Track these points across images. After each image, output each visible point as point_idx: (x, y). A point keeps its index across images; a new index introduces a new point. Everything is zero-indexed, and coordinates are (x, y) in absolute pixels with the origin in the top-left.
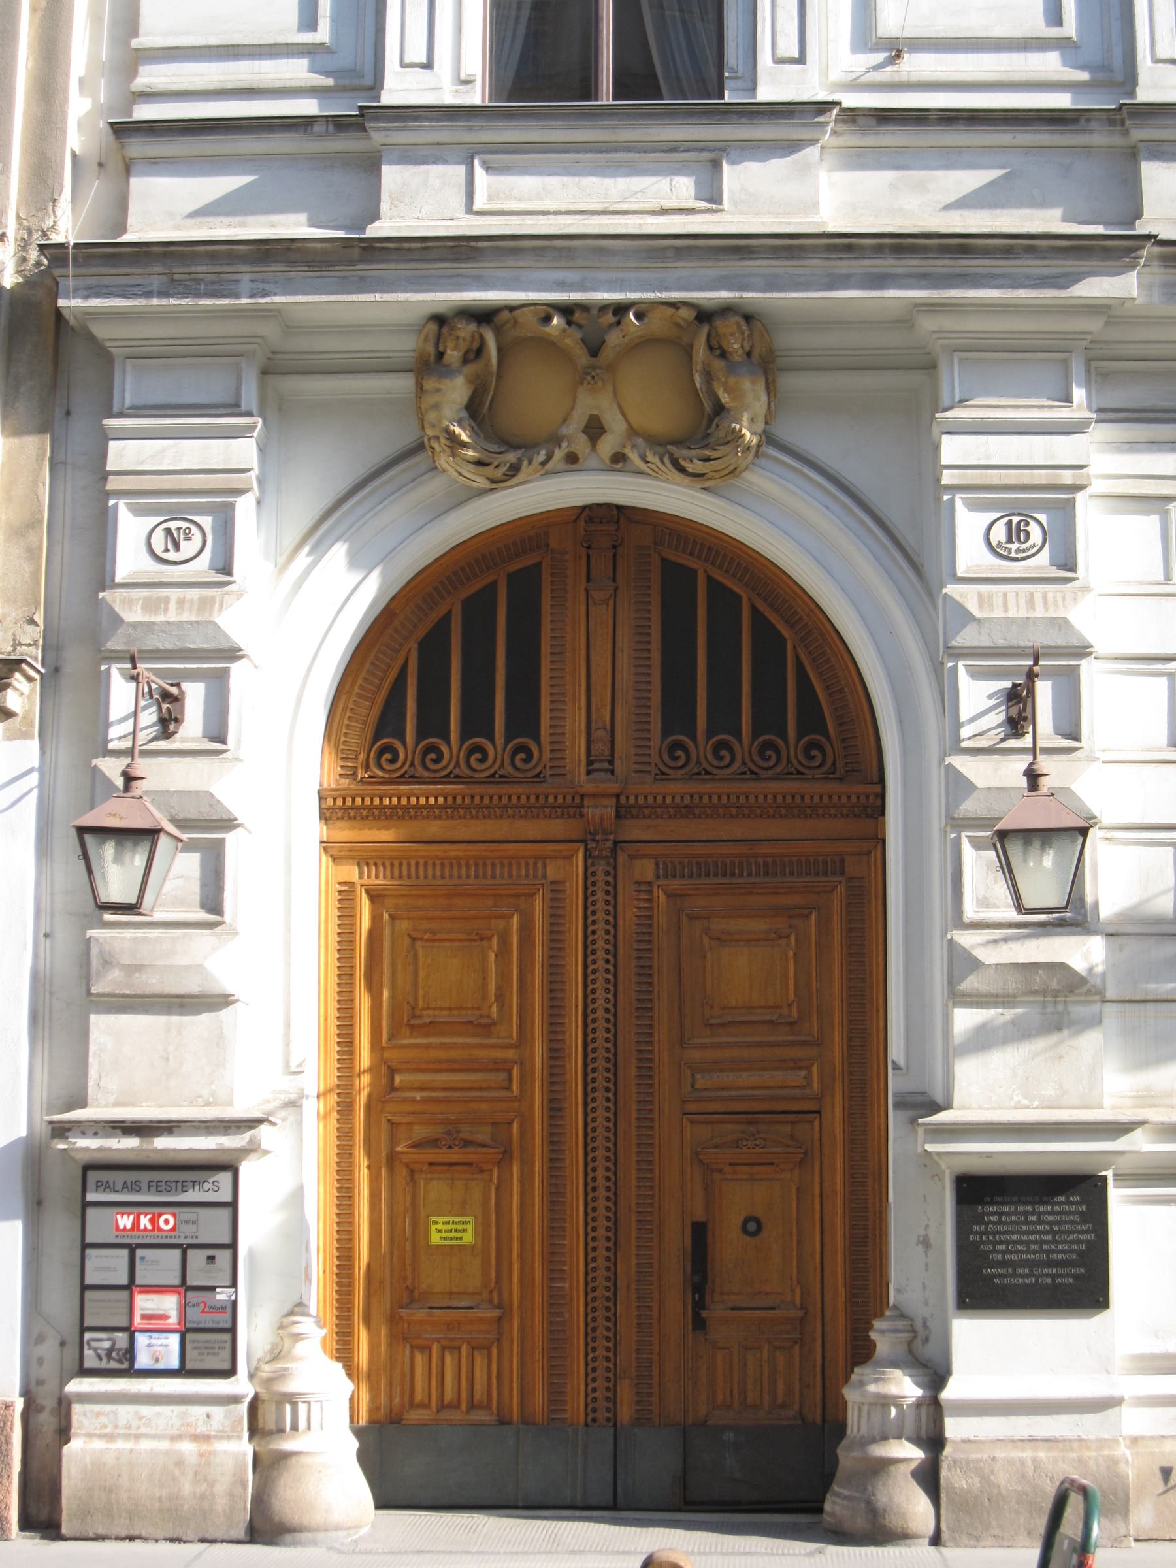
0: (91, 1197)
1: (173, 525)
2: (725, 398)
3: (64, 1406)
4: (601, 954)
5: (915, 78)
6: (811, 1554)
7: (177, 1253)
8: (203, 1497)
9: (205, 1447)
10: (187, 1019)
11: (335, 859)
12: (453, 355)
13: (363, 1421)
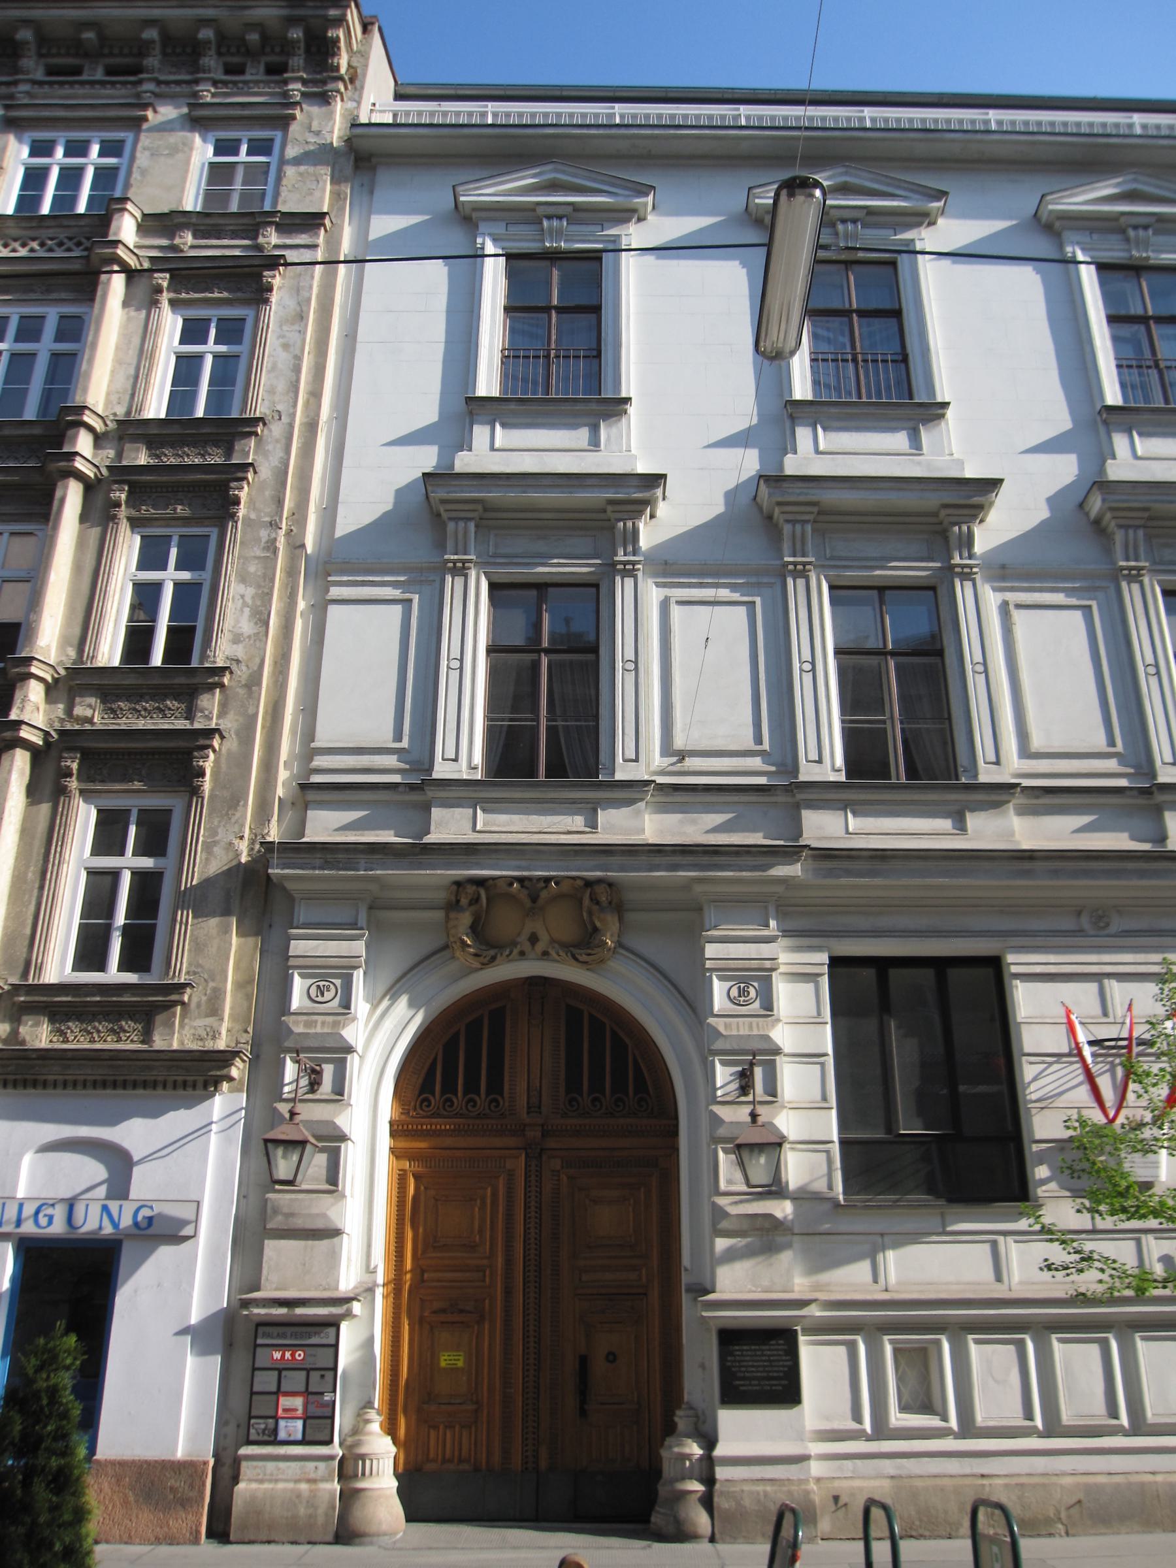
0: (259, 1341)
1: (321, 984)
2: (598, 924)
3: (237, 1462)
4: (533, 1208)
5: (691, 769)
6: (644, 1548)
7: (304, 1373)
8: (310, 1516)
9: (314, 1487)
10: (317, 1242)
11: (397, 1157)
12: (464, 901)
13: (400, 1470)
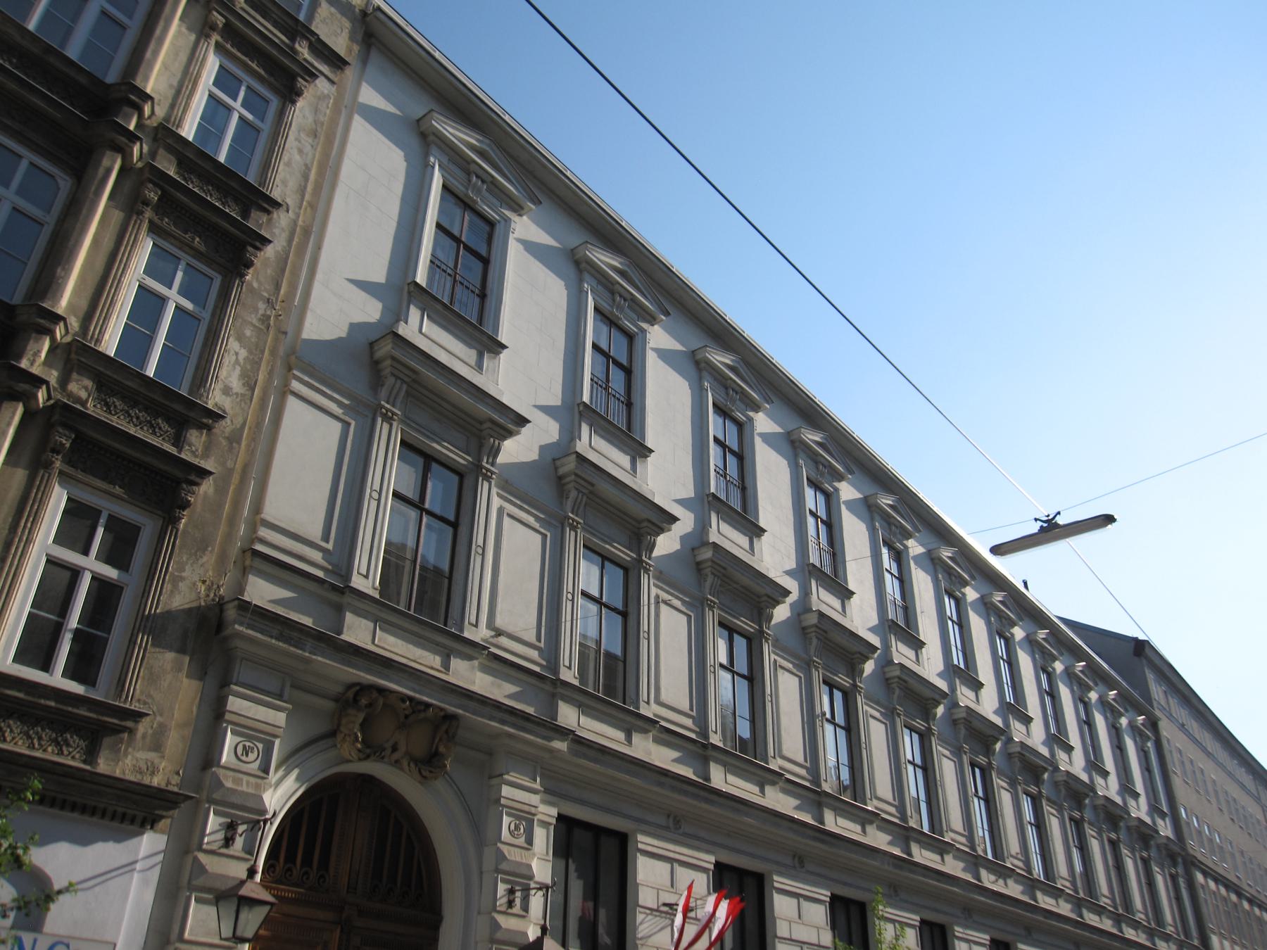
1: (248, 744)
12: (364, 702)
